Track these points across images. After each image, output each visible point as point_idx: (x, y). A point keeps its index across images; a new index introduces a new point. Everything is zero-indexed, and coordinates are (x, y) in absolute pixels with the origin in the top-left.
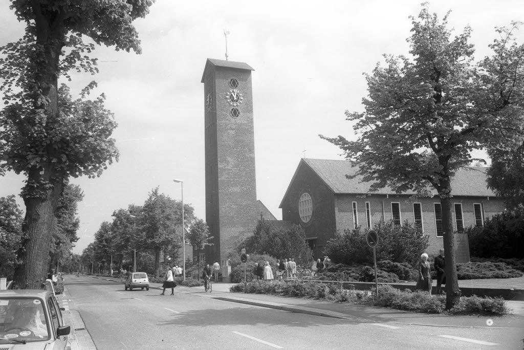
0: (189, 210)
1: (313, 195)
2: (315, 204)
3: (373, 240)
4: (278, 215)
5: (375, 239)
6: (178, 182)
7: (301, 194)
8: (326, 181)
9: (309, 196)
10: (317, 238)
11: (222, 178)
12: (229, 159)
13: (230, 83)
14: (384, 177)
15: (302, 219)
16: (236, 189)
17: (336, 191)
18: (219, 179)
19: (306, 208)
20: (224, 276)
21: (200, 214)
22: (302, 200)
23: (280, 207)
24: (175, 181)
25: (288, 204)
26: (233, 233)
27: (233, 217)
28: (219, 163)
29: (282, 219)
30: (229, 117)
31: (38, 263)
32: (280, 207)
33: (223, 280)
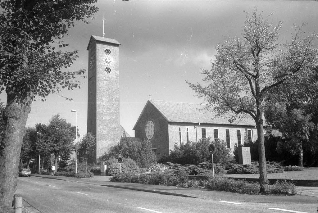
0: (73, 131)
1: (155, 123)
2: (156, 127)
3: (211, 149)
4: (131, 134)
5: (213, 149)
6: (74, 112)
7: (147, 122)
8: (163, 114)
9: (152, 123)
10: (156, 148)
11: (99, 110)
12: (103, 99)
13: (106, 52)
14: (221, 110)
15: (147, 137)
16: (108, 118)
17: (170, 121)
18: (97, 111)
19: (150, 130)
20: (101, 171)
21: (83, 131)
22: (147, 125)
23: (133, 129)
24: (72, 111)
25: (139, 128)
26: (103, 147)
27: (105, 135)
28: (97, 101)
29: (134, 136)
30: (105, 73)
31: (13, 161)
32: (133, 129)
33: (101, 174)
